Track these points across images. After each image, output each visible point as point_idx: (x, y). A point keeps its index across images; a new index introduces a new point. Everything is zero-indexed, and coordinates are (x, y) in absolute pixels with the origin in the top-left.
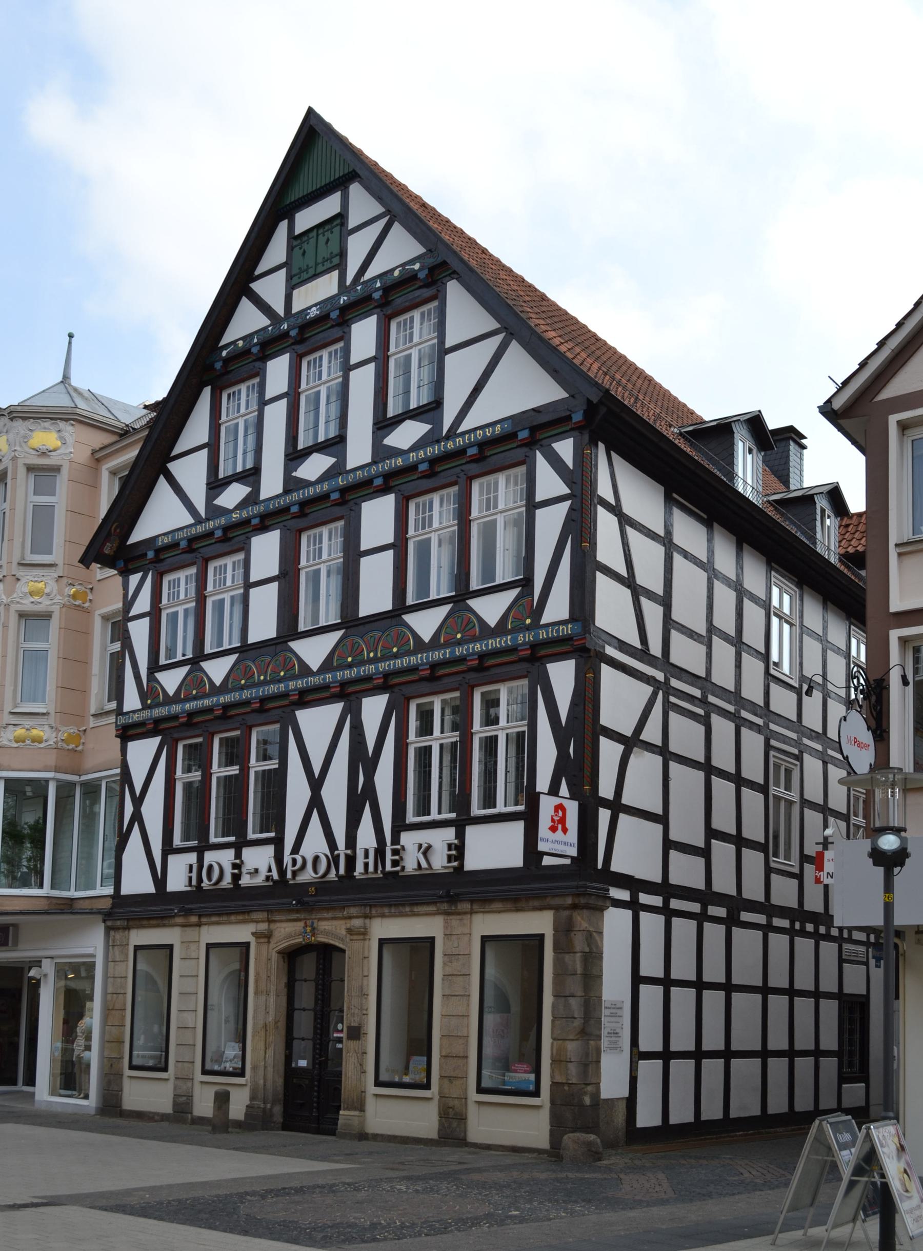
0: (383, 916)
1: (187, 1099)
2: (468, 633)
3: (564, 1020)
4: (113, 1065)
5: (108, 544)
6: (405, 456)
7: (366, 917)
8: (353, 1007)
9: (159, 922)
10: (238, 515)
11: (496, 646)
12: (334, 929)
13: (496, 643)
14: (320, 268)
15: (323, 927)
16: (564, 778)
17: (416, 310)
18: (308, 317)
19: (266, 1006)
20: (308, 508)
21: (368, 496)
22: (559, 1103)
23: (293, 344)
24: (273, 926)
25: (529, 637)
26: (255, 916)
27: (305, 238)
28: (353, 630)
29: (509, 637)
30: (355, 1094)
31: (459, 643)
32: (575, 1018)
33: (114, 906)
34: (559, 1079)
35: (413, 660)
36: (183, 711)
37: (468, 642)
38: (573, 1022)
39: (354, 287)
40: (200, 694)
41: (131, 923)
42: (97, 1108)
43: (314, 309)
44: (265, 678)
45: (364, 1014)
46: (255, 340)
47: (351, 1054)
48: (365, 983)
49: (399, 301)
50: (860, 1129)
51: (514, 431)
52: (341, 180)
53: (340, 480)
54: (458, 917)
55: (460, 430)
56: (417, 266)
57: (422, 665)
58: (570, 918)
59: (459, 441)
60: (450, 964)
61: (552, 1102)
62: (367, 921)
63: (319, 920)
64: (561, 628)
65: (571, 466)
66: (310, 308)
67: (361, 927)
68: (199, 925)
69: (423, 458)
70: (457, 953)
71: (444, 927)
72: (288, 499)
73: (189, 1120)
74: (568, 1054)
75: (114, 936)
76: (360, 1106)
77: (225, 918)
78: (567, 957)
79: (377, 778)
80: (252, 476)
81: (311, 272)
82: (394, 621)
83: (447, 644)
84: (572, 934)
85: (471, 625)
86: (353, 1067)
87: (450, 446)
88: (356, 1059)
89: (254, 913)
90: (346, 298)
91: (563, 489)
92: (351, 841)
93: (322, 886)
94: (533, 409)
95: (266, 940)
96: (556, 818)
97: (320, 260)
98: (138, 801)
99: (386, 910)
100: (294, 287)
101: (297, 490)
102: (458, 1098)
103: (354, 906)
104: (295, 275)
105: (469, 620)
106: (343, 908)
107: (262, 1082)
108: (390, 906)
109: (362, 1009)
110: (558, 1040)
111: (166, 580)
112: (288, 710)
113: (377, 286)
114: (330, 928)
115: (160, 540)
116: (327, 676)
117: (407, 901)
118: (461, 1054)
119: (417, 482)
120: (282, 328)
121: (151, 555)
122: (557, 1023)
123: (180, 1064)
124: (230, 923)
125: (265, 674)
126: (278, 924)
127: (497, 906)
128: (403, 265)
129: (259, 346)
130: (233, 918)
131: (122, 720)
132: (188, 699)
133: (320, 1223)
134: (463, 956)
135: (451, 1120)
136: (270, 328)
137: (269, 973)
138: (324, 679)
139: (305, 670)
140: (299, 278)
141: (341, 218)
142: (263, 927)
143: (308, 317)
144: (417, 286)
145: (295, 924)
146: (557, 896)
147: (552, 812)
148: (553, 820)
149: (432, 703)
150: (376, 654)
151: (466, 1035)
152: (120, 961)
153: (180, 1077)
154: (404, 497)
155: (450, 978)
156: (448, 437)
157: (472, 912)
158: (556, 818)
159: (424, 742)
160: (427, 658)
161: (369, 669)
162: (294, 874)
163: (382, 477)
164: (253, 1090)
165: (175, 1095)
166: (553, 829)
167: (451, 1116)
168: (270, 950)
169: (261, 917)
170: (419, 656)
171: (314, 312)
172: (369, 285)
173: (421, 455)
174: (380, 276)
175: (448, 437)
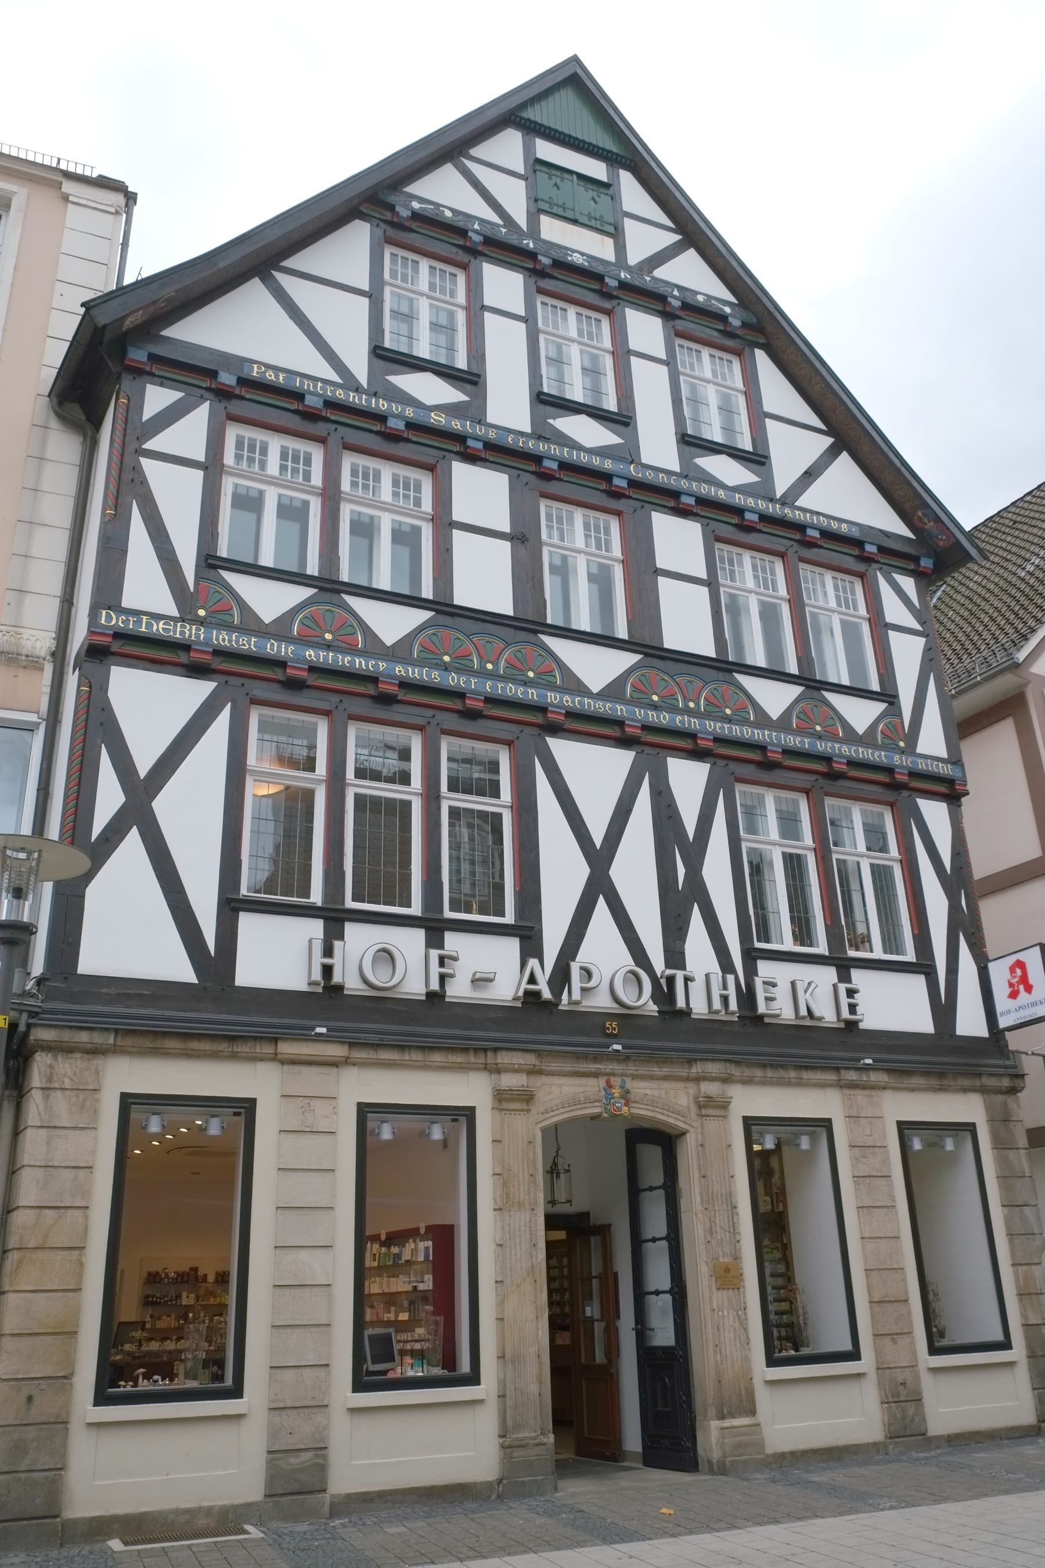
1: (316, 1456)
3: (1024, 1237)
7: (534, 1072)
8: (718, 1229)
12: (663, 1096)
15: (644, 1091)
16: (93, 839)
22: (1040, 1354)
26: (504, 1058)
30: (742, 1385)
32: (1034, 1234)
34: (1034, 1319)
37: (738, 723)
38: (1034, 1240)
40: (209, 620)
47: (726, 1313)
50: (247, 1533)
51: (863, 539)
54: (866, 1092)
58: (1005, 1104)
60: (864, 1160)
61: (1032, 1356)
63: (634, 1077)
70: (872, 1144)
73: (327, 1508)
77: (416, 1056)
78: (1011, 1154)
79: (945, 903)
82: (721, 675)
83: (800, 731)
84: (1011, 1124)
86: (732, 1335)
88: (737, 1321)
89: (504, 1053)
90: (629, 277)
92: (675, 957)
96: (1014, 981)
99: (759, 1073)
102: (908, 1367)
103: (713, 1060)
106: (690, 1062)
108: (764, 1066)
110: (1021, 1265)
114: (656, 1093)
115: (255, 370)
117: (791, 1062)
123: (289, 1376)
124: (425, 1067)
125: (495, 663)
126: (545, 1079)
127: (919, 1081)
128: (709, 297)
130: (437, 1057)
132: (407, 660)
134: (881, 1149)
135: (903, 1404)
147: (1008, 976)
148: (1011, 985)
153: (289, 1404)
155: (868, 1180)
158: (1014, 981)
166: (1014, 995)
167: (902, 1399)
169: (522, 1062)
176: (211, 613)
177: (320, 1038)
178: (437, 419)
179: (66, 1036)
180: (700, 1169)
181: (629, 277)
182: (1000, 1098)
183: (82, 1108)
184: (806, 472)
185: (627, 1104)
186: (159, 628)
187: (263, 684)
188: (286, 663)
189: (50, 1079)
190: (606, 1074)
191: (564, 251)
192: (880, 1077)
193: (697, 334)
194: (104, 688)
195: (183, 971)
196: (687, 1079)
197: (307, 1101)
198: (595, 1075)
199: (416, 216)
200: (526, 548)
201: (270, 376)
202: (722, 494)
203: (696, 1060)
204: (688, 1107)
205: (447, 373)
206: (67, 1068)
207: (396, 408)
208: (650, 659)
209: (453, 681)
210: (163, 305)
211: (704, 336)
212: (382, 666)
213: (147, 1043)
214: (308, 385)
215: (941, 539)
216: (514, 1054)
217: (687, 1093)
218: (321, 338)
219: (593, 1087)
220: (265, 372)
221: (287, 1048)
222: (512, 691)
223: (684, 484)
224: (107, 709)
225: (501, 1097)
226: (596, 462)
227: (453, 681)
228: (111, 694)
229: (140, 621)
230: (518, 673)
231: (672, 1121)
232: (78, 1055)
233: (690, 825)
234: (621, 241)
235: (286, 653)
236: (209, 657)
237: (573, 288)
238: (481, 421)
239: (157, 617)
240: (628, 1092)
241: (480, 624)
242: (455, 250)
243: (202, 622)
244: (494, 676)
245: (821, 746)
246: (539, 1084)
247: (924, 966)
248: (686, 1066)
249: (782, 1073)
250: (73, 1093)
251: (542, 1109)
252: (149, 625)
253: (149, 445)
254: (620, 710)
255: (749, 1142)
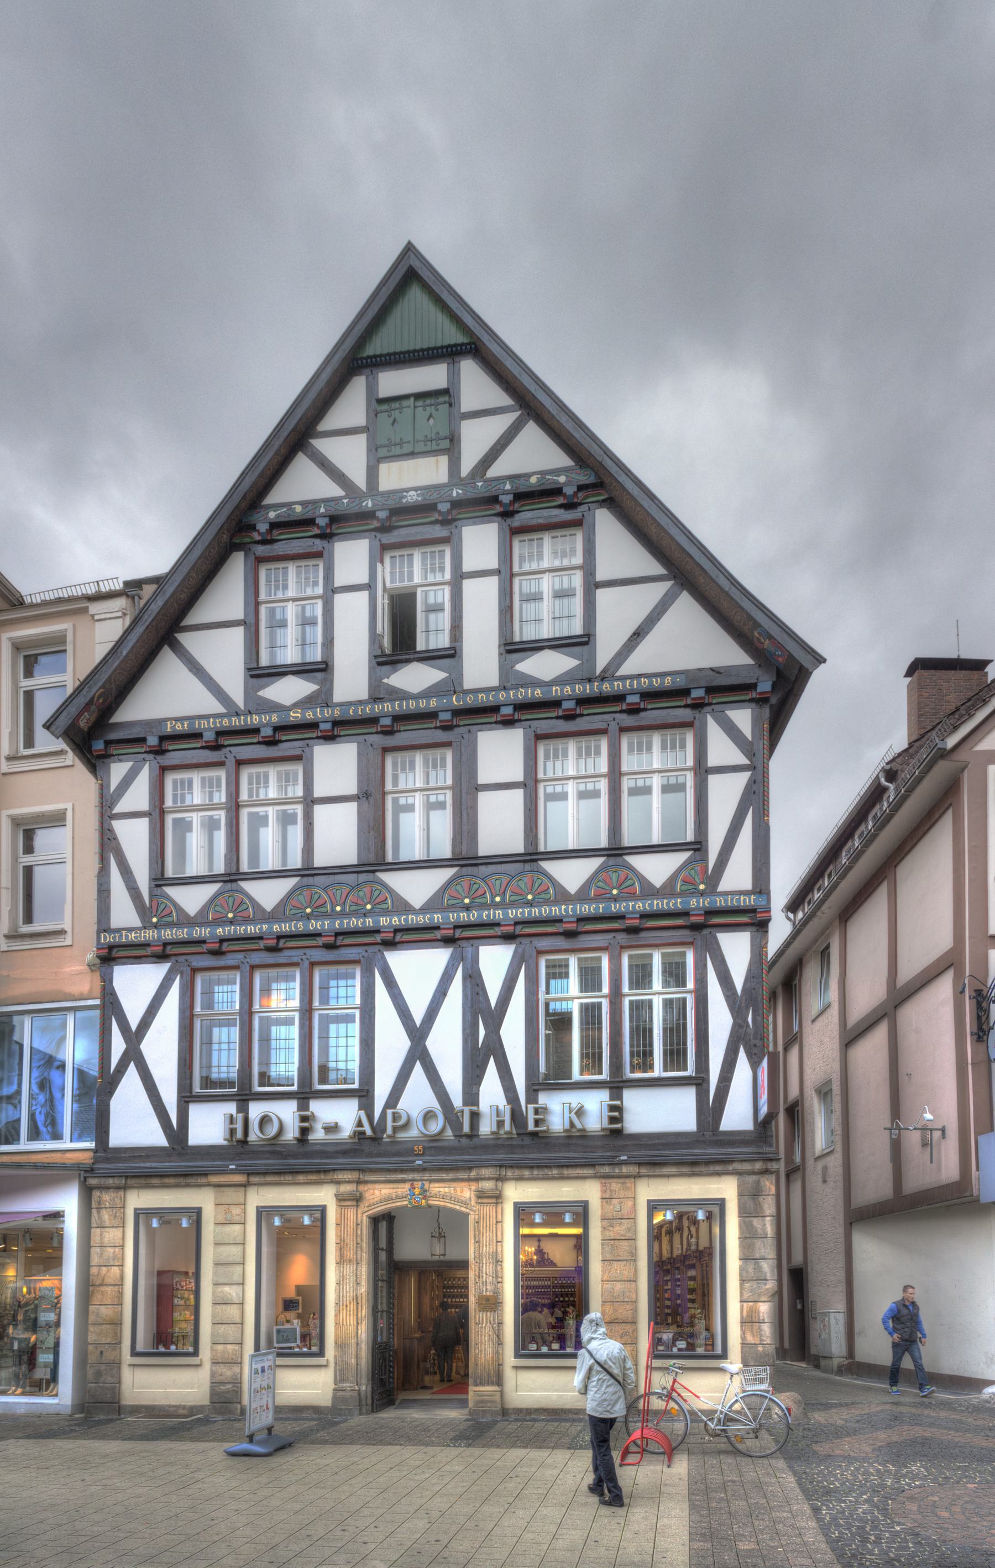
0: (520, 1179)
2: (625, 890)
4: (105, 1353)
5: (86, 714)
6: (545, 689)
9: (181, 1180)
10: (299, 715)
11: (663, 907)
12: (452, 1192)
13: (662, 905)
14: (420, 447)
15: (438, 1189)
17: (547, 533)
18: (404, 501)
19: (357, 1276)
20: (115, 749)
21: (488, 726)
23: (375, 530)
24: (362, 1188)
25: (705, 903)
26: (340, 1176)
27: (396, 405)
28: (466, 870)
29: (679, 900)
31: (615, 899)
32: (766, 1280)
33: (96, 1160)
35: (555, 911)
36: (390, 925)
37: (540, 904)
39: (473, 481)
41: (130, 1182)
42: (73, 1406)
43: (412, 493)
44: (342, 910)
45: (498, 1282)
46: (322, 510)
48: (499, 1249)
49: (403, 531)
51: (689, 687)
52: (416, 354)
53: (454, 699)
55: (621, 672)
56: (562, 479)
57: (154, 941)
59: (618, 686)
60: (611, 1229)
62: (500, 1184)
63: (431, 1181)
64: (742, 898)
65: (750, 737)
66: (407, 490)
67: (492, 1190)
68: (245, 1185)
69: (569, 695)
71: (601, 1191)
72: (377, 708)
74: (761, 1315)
75: (100, 1197)
76: (498, 1379)
78: (756, 1222)
79: (504, 1032)
80: (451, 655)
81: (407, 448)
82: (528, 866)
83: (599, 898)
84: (761, 1199)
85: (244, 907)
87: (606, 688)
90: (460, 492)
91: (740, 758)
92: (471, 1096)
93: (433, 1144)
94: (711, 669)
95: (354, 1203)
97: (420, 436)
98: (134, 1038)
99: (527, 1173)
100: (380, 460)
101: (392, 701)
104: (382, 446)
105: (242, 903)
106: (470, 1169)
107: (353, 1361)
109: (497, 1277)
111: (170, 779)
112: (376, 948)
113: (506, 488)
115: (169, 726)
116: (436, 916)
118: (630, 1320)
119: (554, 721)
120: (364, 504)
121: (153, 741)
122: (747, 1285)
125: (503, 895)
126: (370, 1186)
128: (543, 473)
129: (388, 511)
130: (301, 1178)
131: (108, 939)
133: (899, 1524)
136: (345, 501)
137: (359, 1240)
138: (431, 919)
139: (404, 907)
140: (389, 451)
141: (447, 395)
142: (346, 1188)
143: (404, 501)
144: (433, 519)
145: (401, 1185)
146: (745, 1161)
149: (650, 956)
150: (503, 899)
151: (634, 1300)
152: (113, 1227)
153: (220, 1361)
154: (161, 767)
155: (612, 1242)
156: (603, 679)
157: (638, 1176)
159: (640, 996)
160: (574, 910)
161: (494, 914)
162: (395, 1129)
163: (704, 689)
164: (341, 1370)
165: (212, 1383)
168: (359, 1215)
170: (563, 907)
171: (412, 497)
172: (493, 485)
173: (567, 691)
174: (512, 478)
175: (603, 679)
176: (160, 919)
177: (233, 1172)
178: (295, 716)
179: (103, 1181)
180: (475, 1237)
181: (460, 492)
182: (751, 1179)
183: (115, 1217)
184: (634, 634)
185: (425, 1198)
186: (132, 936)
187: (199, 957)
188: (756, 909)
189: (99, 1204)
190: (410, 1180)
191: (400, 494)
192: (633, 1169)
193: (534, 522)
194: (111, 982)
195: (158, 1138)
196: (469, 1180)
197: (227, 1207)
198: (404, 1181)
199: (274, 525)
200: (369, 803)
201: (179, 727)
202: (412, 705)
203: (473, 1167)
204: (470, 1198)
205: (302, 670)
206: (107, 1197)
207: (265, 719)
208: (464, 869)
209: (312, 926)
210: (101, 701)
211: (541, 521)
212: (265, 927)
213: (143, 1181)
214: (204, 724)
215: (779, 656)
216: (345, 1172)
217: (470, 1189)
218: (211, 679)
219: (404, 1189)
220: (175, 726)
221: (214, 1179)
222: (355, 923)
223: (377, 708)
224: (113, 994)
225: (340, 1198)
226: (423, 704)
227: (312, 926)
228: (115, 984)
229: (121, 936)
230: (520, 898)
231: (457, 1207)
232: (111, 1190)
233: (493, 994)
234: (456, 451)
235: (205, 934)
236: (575, 925)
237: (295, 543)
238: (327, 704)
239: (130, 930)
240: (425, 1191)
241: (331, 876)
242: (310, 541)
243: (156, 926)
244: (343, 914)
245: (512, 914)
246: (366, 1188)
247: (700, 1082)
248: (468, 1171)
249: (546, 1171)
250: (110, 1210)
251: (367, 1204)
252: (127, 937)
253: (116, 810)
254: (437, 918)
255: (650, 1217)
